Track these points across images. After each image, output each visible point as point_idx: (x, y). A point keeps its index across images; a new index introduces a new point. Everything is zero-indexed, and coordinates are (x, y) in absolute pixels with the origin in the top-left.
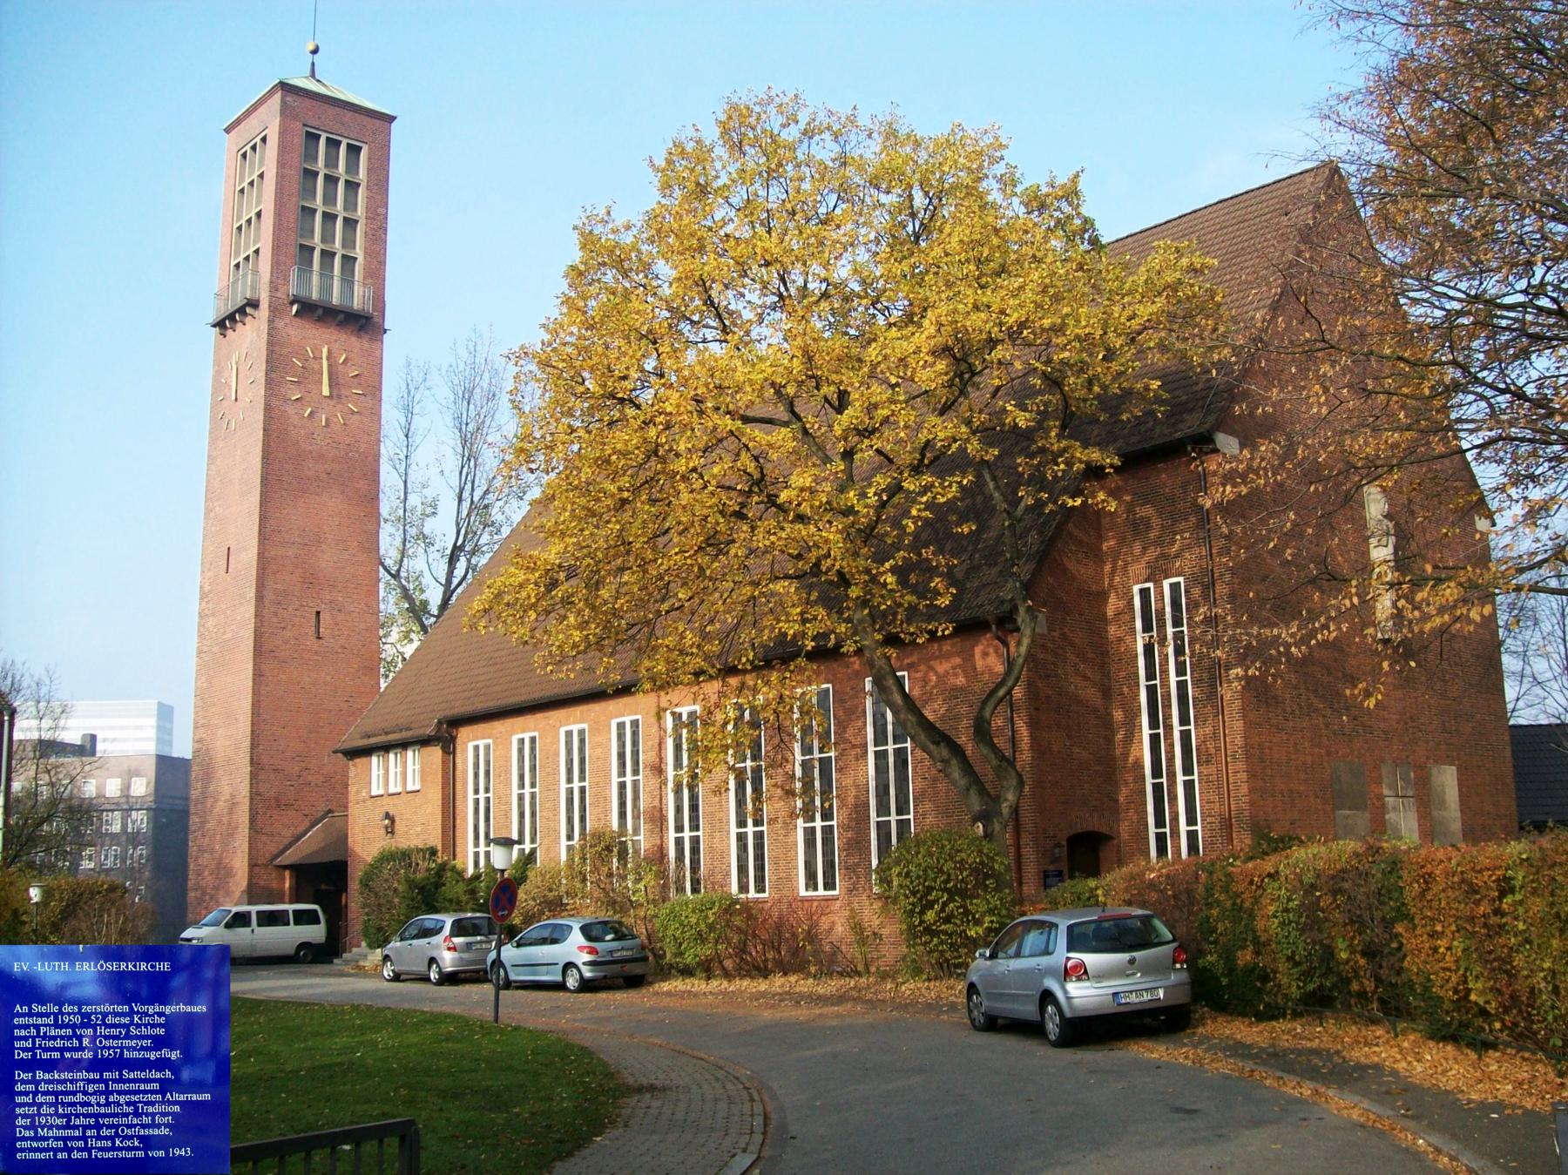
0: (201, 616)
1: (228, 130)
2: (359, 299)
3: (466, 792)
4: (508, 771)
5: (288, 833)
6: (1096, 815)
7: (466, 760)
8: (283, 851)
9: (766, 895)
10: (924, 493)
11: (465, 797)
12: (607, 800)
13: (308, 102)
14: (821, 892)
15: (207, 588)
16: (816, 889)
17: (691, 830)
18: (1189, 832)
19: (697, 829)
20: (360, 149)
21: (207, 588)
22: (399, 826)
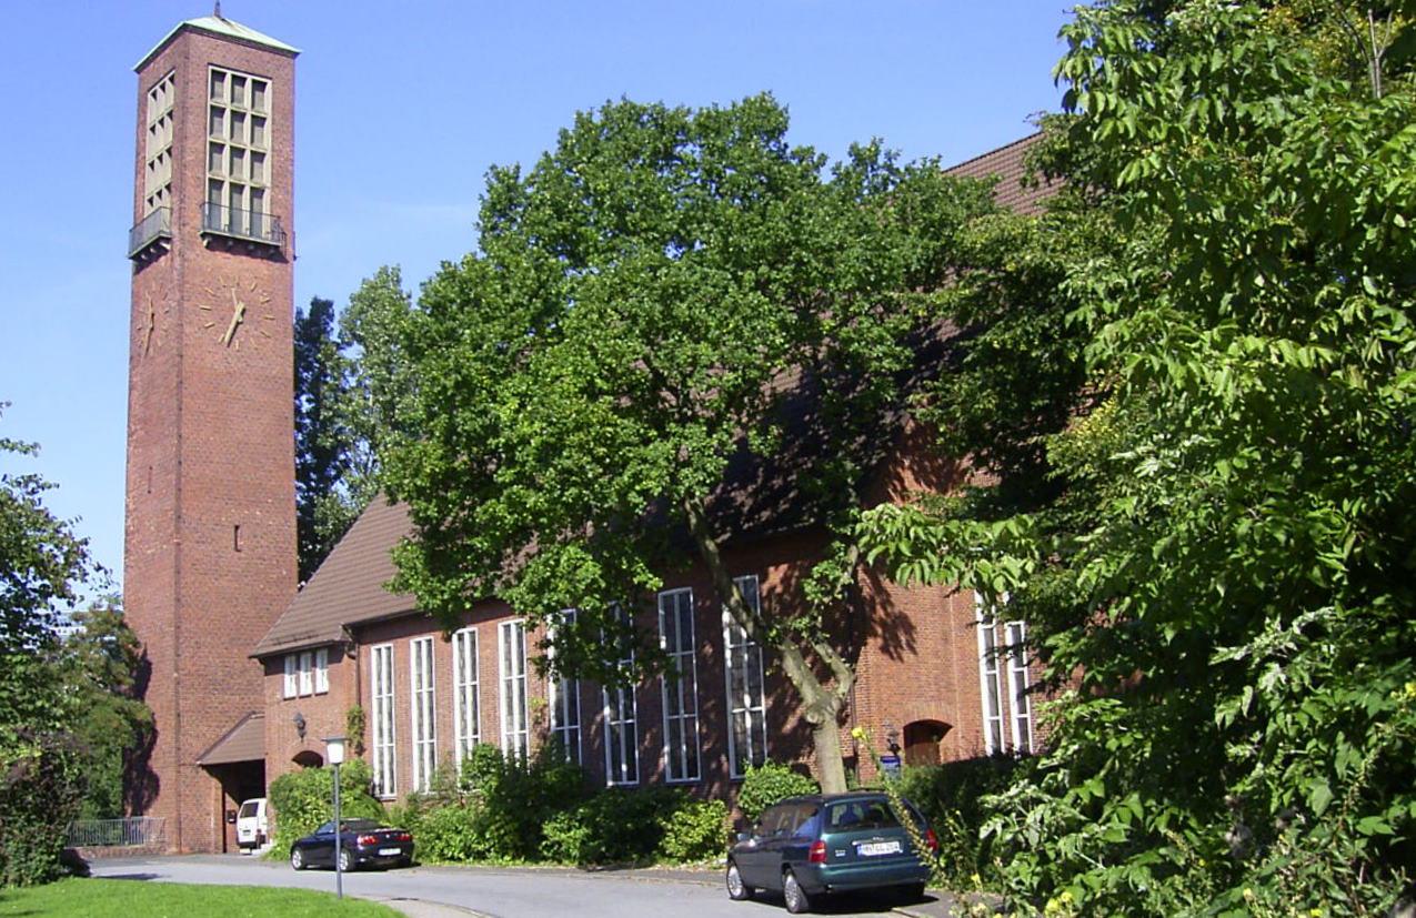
0: (127, 534)
1: (138, 71)
2: (265, 235)
3: (370, 692)
4: (408, 672)
5: (211, 736)
6: (933, 704)
7: (369, 664)
8: (208, 752)
9: (637, 782)
10: (1199, 450)
11: (370, 697)
12: (496, 697)
13: (267, 56)
14: (685, 779)
15: (131, 507)
16: (681, 776)
17: (571, 724)
18: (671, 721)
19: (1025, 712)
20: (265, 84)
21: (131, 507)
22: (308, 728)
